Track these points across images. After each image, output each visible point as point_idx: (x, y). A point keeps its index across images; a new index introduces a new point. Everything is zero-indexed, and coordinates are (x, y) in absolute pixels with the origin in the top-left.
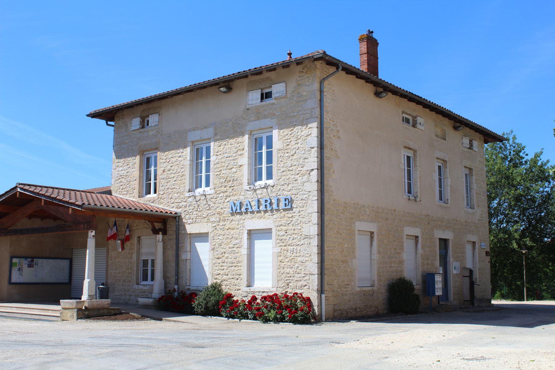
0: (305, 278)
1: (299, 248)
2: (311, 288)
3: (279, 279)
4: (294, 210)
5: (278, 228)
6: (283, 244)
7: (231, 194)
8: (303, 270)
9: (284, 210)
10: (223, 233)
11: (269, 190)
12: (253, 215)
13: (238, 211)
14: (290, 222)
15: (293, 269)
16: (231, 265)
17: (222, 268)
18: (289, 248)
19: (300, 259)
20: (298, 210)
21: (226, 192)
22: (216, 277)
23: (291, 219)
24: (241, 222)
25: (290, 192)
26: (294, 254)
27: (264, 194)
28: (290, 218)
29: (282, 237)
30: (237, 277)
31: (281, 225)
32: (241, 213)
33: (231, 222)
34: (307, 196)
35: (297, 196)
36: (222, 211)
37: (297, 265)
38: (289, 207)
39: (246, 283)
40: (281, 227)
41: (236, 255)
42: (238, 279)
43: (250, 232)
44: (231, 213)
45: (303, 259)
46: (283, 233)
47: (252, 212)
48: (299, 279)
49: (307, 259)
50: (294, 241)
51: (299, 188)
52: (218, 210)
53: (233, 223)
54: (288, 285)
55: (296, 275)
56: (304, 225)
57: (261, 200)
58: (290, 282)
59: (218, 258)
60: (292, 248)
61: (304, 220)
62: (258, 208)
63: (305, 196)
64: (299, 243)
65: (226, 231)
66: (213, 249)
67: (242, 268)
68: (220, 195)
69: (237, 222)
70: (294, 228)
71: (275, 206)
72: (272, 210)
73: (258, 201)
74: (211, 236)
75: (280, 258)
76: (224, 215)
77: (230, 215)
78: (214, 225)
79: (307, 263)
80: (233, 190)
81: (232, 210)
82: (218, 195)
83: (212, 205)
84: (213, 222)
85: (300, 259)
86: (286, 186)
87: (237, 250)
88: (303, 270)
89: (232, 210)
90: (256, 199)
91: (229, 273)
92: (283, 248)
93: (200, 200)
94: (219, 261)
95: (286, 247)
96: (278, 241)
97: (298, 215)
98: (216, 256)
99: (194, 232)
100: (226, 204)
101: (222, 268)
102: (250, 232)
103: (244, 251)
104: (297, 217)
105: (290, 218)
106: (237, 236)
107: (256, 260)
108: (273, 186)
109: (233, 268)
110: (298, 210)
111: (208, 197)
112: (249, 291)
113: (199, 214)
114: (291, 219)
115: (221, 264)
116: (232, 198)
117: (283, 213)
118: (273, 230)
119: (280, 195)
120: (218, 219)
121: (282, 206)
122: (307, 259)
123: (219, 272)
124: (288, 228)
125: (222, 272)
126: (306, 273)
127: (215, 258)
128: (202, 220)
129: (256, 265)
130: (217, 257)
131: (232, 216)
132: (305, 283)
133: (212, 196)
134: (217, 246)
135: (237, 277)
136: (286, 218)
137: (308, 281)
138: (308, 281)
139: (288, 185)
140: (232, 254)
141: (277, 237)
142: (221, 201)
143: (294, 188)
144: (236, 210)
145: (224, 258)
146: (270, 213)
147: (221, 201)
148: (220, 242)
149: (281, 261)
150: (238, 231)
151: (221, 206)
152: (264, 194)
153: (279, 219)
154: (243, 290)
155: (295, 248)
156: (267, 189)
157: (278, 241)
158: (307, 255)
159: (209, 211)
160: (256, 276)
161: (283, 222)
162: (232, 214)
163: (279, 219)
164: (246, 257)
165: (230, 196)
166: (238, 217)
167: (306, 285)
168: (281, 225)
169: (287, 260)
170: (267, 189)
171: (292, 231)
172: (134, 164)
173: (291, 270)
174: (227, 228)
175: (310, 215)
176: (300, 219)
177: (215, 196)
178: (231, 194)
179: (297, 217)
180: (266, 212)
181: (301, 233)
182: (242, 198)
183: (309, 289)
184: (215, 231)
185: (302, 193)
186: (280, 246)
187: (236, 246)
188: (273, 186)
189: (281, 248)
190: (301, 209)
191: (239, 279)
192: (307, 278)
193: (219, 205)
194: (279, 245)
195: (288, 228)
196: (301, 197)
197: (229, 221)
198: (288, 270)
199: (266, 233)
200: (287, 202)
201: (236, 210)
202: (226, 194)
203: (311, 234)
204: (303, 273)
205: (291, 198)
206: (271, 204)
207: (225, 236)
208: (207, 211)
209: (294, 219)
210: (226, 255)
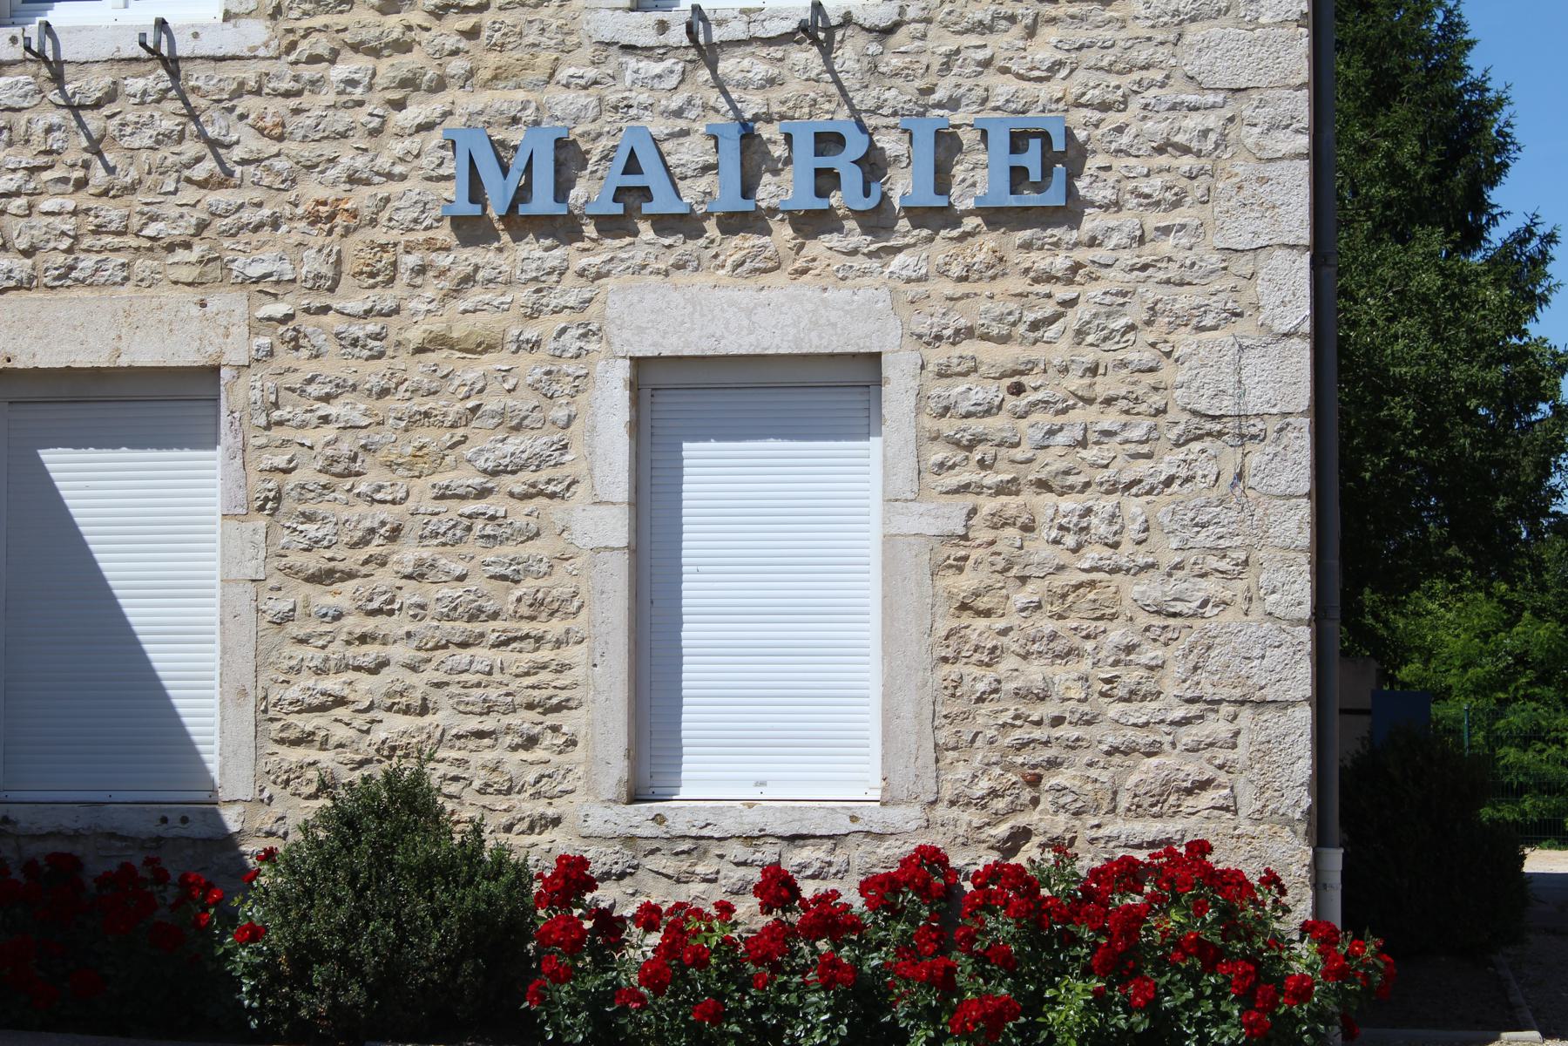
0: (1187, 736)
1: (1134, 507)
2: (1248, 802)
3: (944, 736)
4: (1092, 222)
5: (939, 355)
6: (991, 479)
7: (457, 66)
8: (1176, 670)
9: (995, 217)
10: (373, 373)
11: (848, 55)
12: (685, 247)
13: (542, 202)
14: (1050, 308)
15: (1085, 666)
16: (460, 628)
17: (372, 652)
18: (1046, 503)
19: (1148, 588)
20: (1128, 220)
21: (402, 47)
22: (308, 722)
23: (1062, 292)
24: (570, 292)
25: (1055, 88)
26: (1092, 555)
27: (794, 87)
28: (1049, 278)
29: (977, 426)
30: (524, 721)
31: (969, 333)
32: (563, 229)
33: (457, 291)
34: (1212, 120)
35: (1114, 118)
36: (361, 198)
37: (1117, 634)
38: (1054, 196)
39: (617, 770)
40: (968, 348)
41: (509, 550)
42: (531, 742)
43: (651, 378)
44: (458, 223)
45: (1173, 587)
46: (992, 391)
47: (683, 224)
48: (1143, 738)
49: (1211, 586)
50: (1091, 453)
51: (1142, 54)
52: (312, 190)
53: (475, 296)
54: (1035, 781)
55: (1114, 710)
56: (1185, 340)
57: (765, 131)
58: (1053, 764)
59: (323, 577)
60: (1069, 504)
61: (1185, 299)
62: (748, 191)
63: (1194, 122)
64: (1141, 468)
65: (403, 360)
66: (271, 504)
67: (568, 654)
68: (339, 72)
69: (524, 295)
70: (1089, 356)
71: (903, 186)
72: (877, 220)
73: (748, 136)
74: (237, 395)
75: (965, 583)
76: (380, 235)
77: (445, 234)
78: (279, 309)
79: (1216, 620)
80: (472, 34)
81: (476, 191)
82: (308, 72)
83: (249, 143)
84: (266, 285)
85: (1148, 588)
86: (1002, 42)
87: (520, 514)
88: (1176, 670)
89: (476, 191)
90: (722, 120)
91: (435, 695)
92: (988, 505)
93: (111, 96)
94: (342, 596)
95: (1011, 503)
96: (939, 453)
97: (1128, 258)
98: (296, 559)
99: (44, 362)
100: (398, 147)
101: (372, 652)
102: (651, 378)
103: (600, 522)
104: (1115, 279)
105: (1049, 278)
106: (523, 402)
107: (694, 591)
108: (888, 31)
109: (483, 655)
110: (1128, 220)
111: (197, 76)
112: (649, 830)
113: (112, 212)
114: (1062, 292)
115: (356, 624)
116: (467, 102)
117: (989, 241)
118: (888, 371)
119: (953, 104)
120: (313, 263)
121: (978, 179)
122: (1211, 586)
123: (333, 684)
124: (1038, 352)
125: (365, 687)
126: (1208, 692)
127: (291, 571)
128: (143, 265)
129: (691, 634)
130: (313, 562)
131: (466, 242)
132: (1194, 769)
133: (249, 73)
134: (307, 474)
135: (524, 721)
136: (1019, 284)
137: (1222, 756)
138: (1222, 756)
139: (1031, 32)
140: (471, 546)
141: (929, 423)
142: (343, 119)
143: (1090, 57)
144: (523, 193)
145: (384, 579)
146: (855, 237)
147: (343, 119)
148: (346, 447)
149: (959, 605)
150: (530, 367)
151: (349, 159)
152: (794, 87)
153: (950, 288)
154: (595, 825)
155: (1106, 504)
156: (826, 49)
157: (939, 453)
158: (1213, 562)
159: (220, 198)
160: (696, 715)
161: (990, 302)
162: (472, 230)
163: (950, 288)
164: (617, 571)
165: (440, 85)
166: (533, 252)
167: (1204, 785)
168: (969, 333)
169: (1022, 597)
170: (826, 49)
171: (1075, 382)
172: (706, 224)
173: (1064, 676)
174: (415, 335)
175: (1243, 265)
176: (1152, 292)
177: (284, 74)
178: (457, 66)
179: (1115, 279)
180: (811, 223)
181: (1157, 400)
182: (563, 101)
183: (1230, 808)
184: (285, 357)
185: (1169, 96)
186: (964, 489)
187: (516, 483)
188: (888, 31)
189: (969, 500)
190: (1154, 219)
191: (548, 739)
192: (1216, 727)
193: (328, 149)
194: (952, 480)
195: (1038, 352)
196: (1156, 128)
197: (432, 288)
198: (1035, 673)
199: (826, 391)
200: (1032, 159)
201: (523, 193)
202: (390, 67)
203: (1253, 404)
204: (1171, 689)
205: (1069, 134)
206: (873, 165)
207: (395, 404)
208: (189, 194)
209: (1094, 291)
210: (408, 554)
